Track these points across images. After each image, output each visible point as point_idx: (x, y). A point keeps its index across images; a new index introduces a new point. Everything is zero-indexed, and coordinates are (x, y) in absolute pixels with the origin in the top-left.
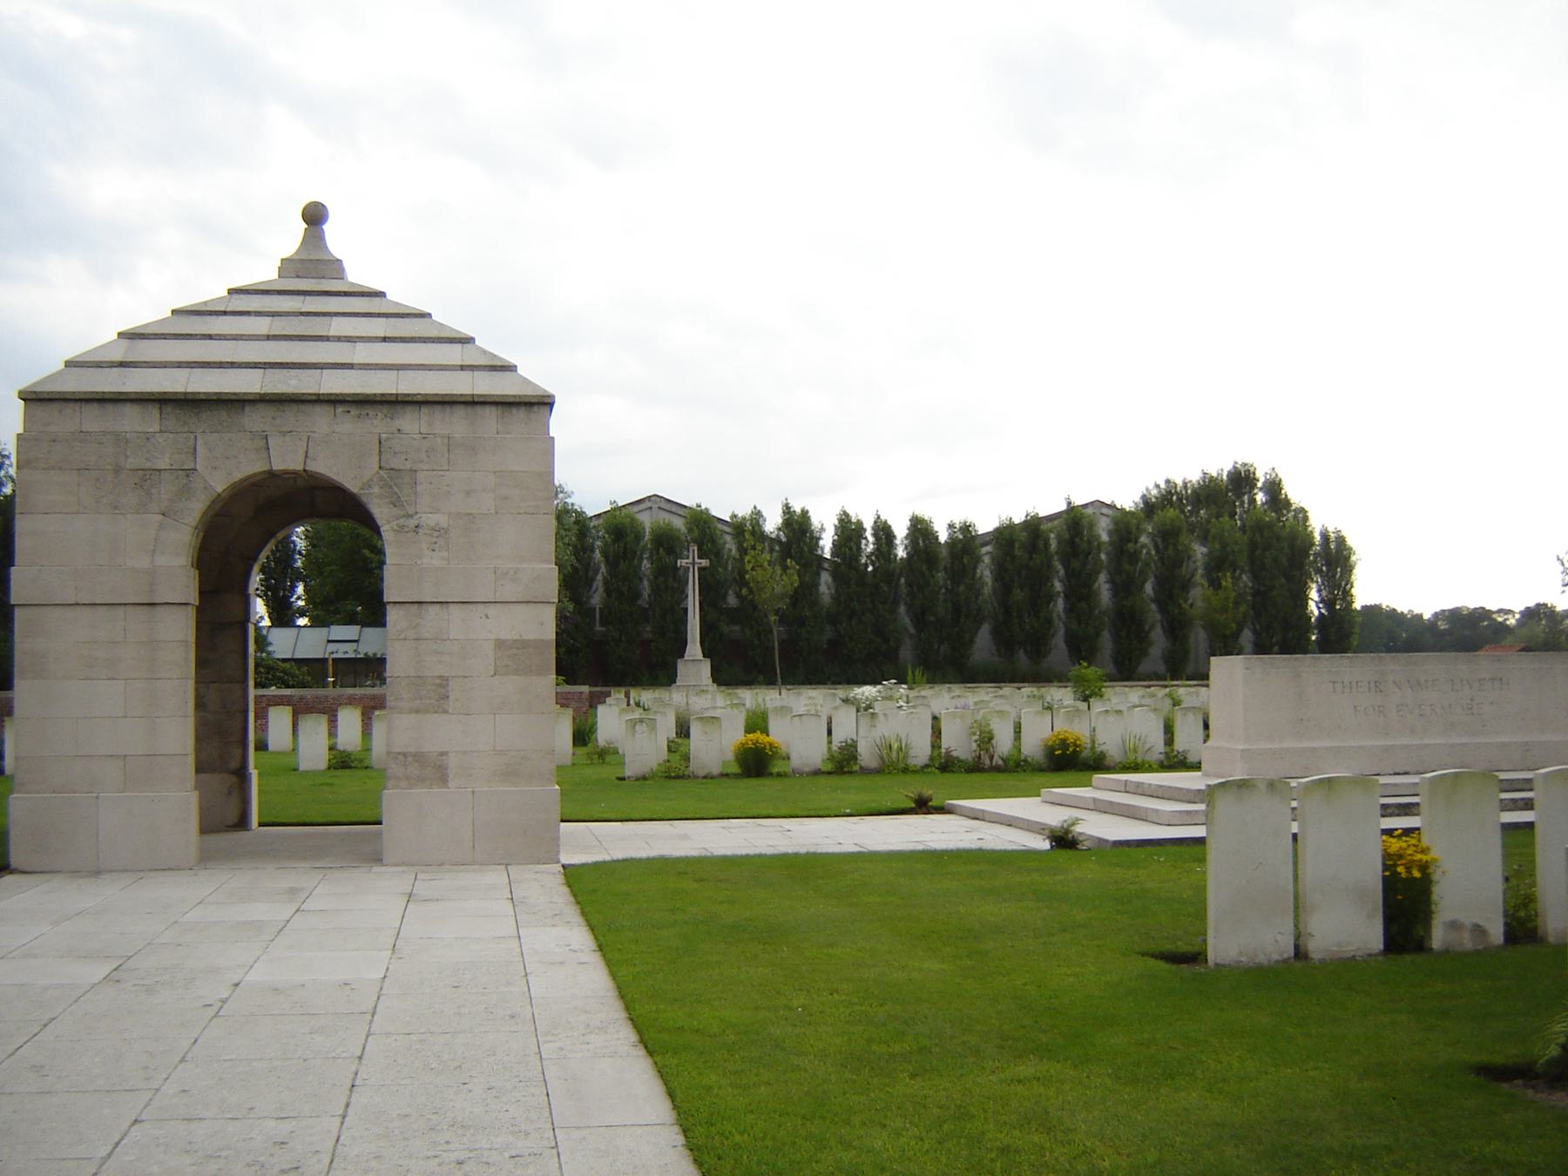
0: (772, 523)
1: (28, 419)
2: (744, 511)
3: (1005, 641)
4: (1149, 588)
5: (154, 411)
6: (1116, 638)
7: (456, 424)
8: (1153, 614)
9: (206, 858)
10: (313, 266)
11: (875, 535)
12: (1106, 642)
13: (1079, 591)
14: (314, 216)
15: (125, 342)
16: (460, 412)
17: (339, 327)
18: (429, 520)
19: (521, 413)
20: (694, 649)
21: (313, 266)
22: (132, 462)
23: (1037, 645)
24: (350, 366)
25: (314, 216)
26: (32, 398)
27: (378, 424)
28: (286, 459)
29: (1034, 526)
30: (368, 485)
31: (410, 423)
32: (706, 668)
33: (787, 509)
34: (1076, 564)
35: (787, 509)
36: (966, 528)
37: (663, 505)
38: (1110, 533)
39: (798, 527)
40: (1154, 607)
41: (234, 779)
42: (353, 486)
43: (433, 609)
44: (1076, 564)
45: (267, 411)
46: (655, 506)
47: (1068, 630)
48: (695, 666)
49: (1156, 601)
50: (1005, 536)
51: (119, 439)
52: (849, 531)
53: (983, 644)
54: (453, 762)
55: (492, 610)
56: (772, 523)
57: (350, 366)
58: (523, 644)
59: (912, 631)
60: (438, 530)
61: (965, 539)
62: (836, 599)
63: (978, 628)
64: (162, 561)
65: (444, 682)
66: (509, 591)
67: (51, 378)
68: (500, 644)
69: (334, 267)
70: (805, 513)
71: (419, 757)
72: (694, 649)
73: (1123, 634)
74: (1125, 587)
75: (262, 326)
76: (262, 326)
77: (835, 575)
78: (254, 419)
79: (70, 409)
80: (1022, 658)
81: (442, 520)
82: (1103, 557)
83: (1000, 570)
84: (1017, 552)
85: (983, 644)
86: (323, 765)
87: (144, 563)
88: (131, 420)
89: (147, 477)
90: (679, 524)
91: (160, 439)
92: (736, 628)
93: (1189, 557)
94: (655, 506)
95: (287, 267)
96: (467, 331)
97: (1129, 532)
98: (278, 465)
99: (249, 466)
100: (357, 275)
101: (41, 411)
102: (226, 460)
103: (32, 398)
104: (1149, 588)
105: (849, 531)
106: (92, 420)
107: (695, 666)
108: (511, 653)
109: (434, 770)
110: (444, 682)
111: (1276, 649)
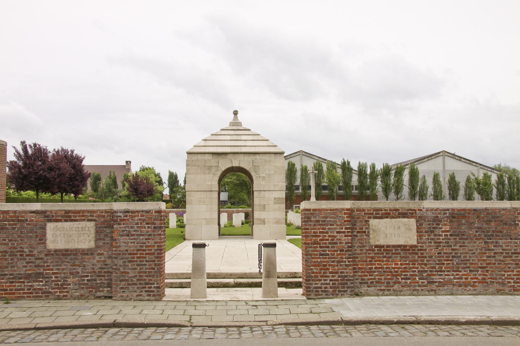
1: (188, 157)
5: (211, 155)
7: (266, 157)
9: (219, 239)
10: (236, 125)
14: (236, 113)
15: (204, 141)
16: (267, 155)
17: (243, 138)
18: (262, 175)
19: (279, 155)
21: (236, 125)
22: (208, 165)
24: (246, 146)
25: (236, 113)
26: (188, 153)
27: (252, 157)
28: (236, 164)
30: (250, 169)
31: (258, 157)
42: (248, 169)
43: (263, 192)
45: (232, 155)
51: (205, 161)
54: (266, 220)
55: (273, 192)
57: (246, 146)
58: (279, 198)
60: (264, 177)
62: (343, 190)
64: (213, 183)
65: (264, 205)
66: (277, 189)
67: (192, 149)
68: (275, 198)
69: (240, 124)
71: (260, 219)
75: (228, 138)
76: (228, 138)
78: (229, 156)
79: (196, 155)
81: (264, 175)
87: (210, 183)
88: (207, 157)
89: (210, 168)
91: (212, 160)
95: (232, 124)
96: (267, 139)
98: (234, 165)
99: (229, 166)
100: (245, 126)
101: (190, 155)
102: (225, 164)
103: (188, 153)
106: (200, 157)
108: (277, 200)
109: (263, 222)
110: (264, 205)
111: (156, 200)
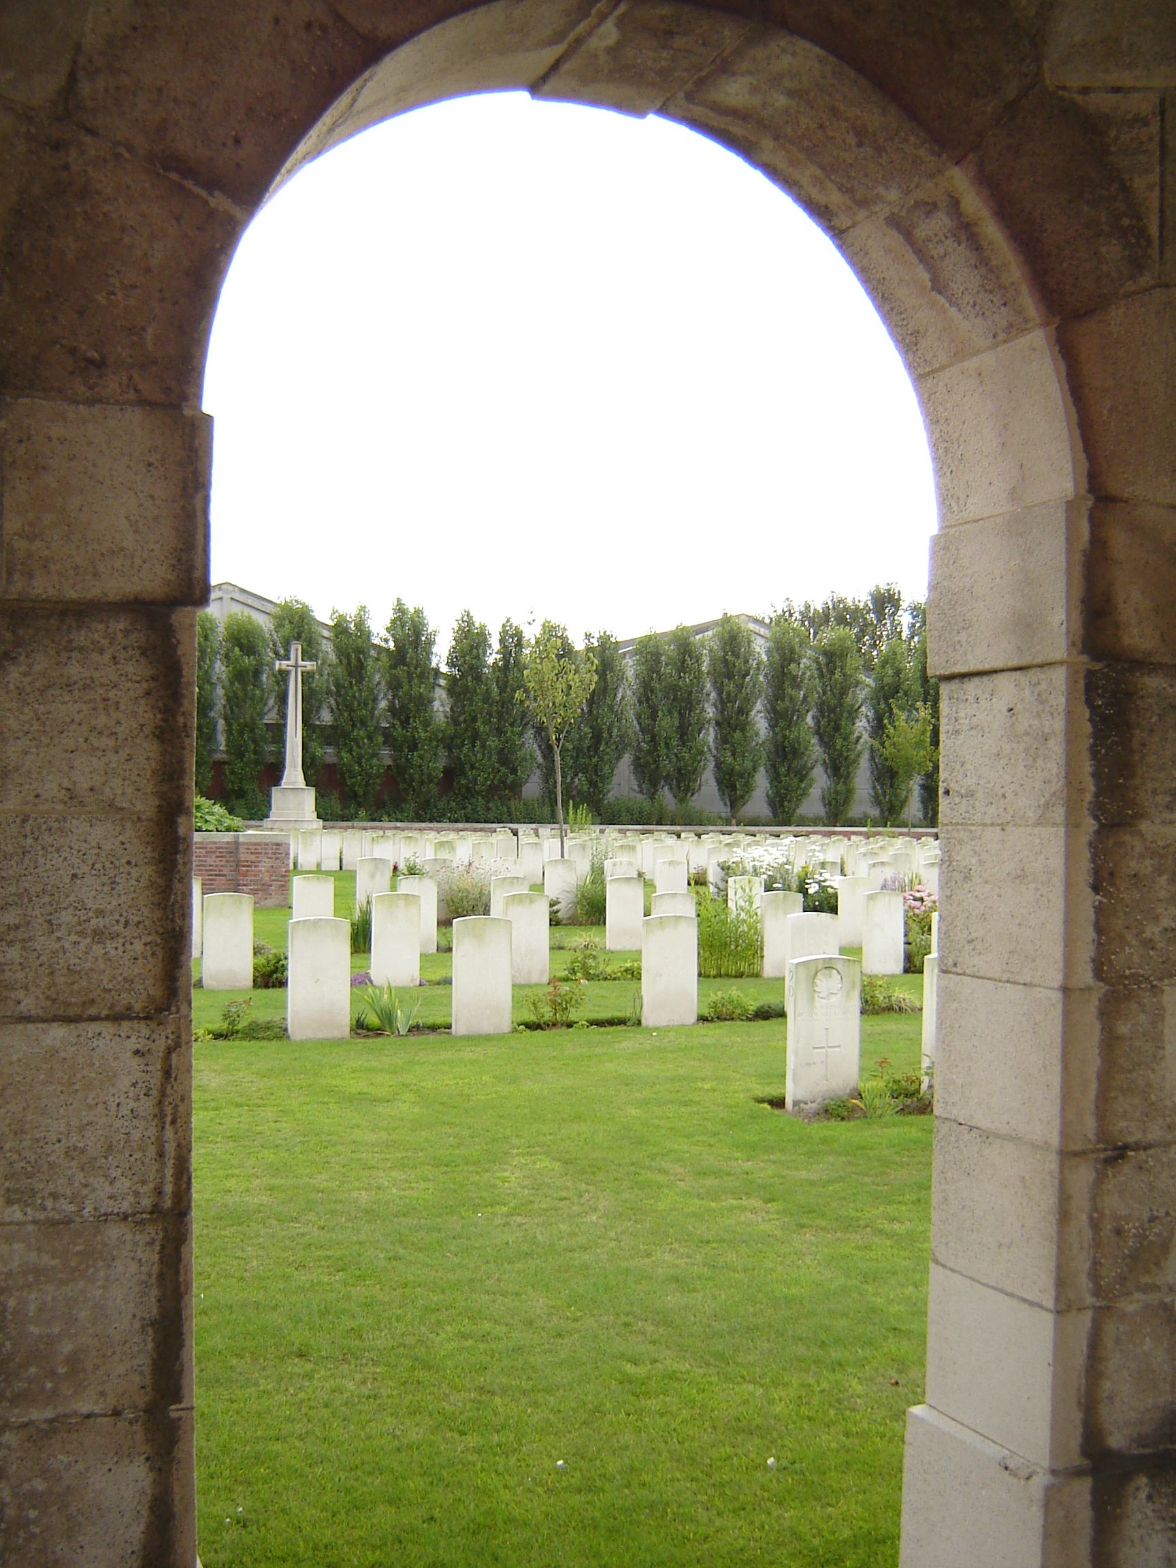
0: (379, 628)
2: (349, 610)
3: (649, 774)
4: (809, 719)
6: (775, 777)
8: (815, 751)
11: (502, 641)
12: (761, 782)
13: (732, 724)
20: (294, 774)
23: (684, 782)
29: (683, 642)
32: (310, 796)
33: (400, 609)
34: (730, 687)
35: (400, 609)
36: (605, 640)
37: (237, 596)
38: (769, 652)
39: (411, 633)
40: (814, 740)
41: (1114, 488)
44: (730, 687)
46: (226, 596)
47: (718, 766)
48: (294, 799)
49: (818, 732)
50: (648, 650)
52: (470, 640)
53: (623, 781)
56: (379, 628)
59: (540, 760)
61: (605, 654)
62: (455, 721)
63: (619, 758)
70: (418, 612)
72: (294, 774)
73: (783, 770)
74: (780, 717)
77: (451, 691)
80: (666, 796)
82: (761, 678)
83: (646, 692)
84: (666, 670)
85: (623, 781)
86: (505, 1025)
90: (264, 623)
92: (330, 750)
93: (1074, 644)
94: (226, 596)
97: (792, 651)
104: (809, 719)
105: (470, 640)
107: (294, 799)
